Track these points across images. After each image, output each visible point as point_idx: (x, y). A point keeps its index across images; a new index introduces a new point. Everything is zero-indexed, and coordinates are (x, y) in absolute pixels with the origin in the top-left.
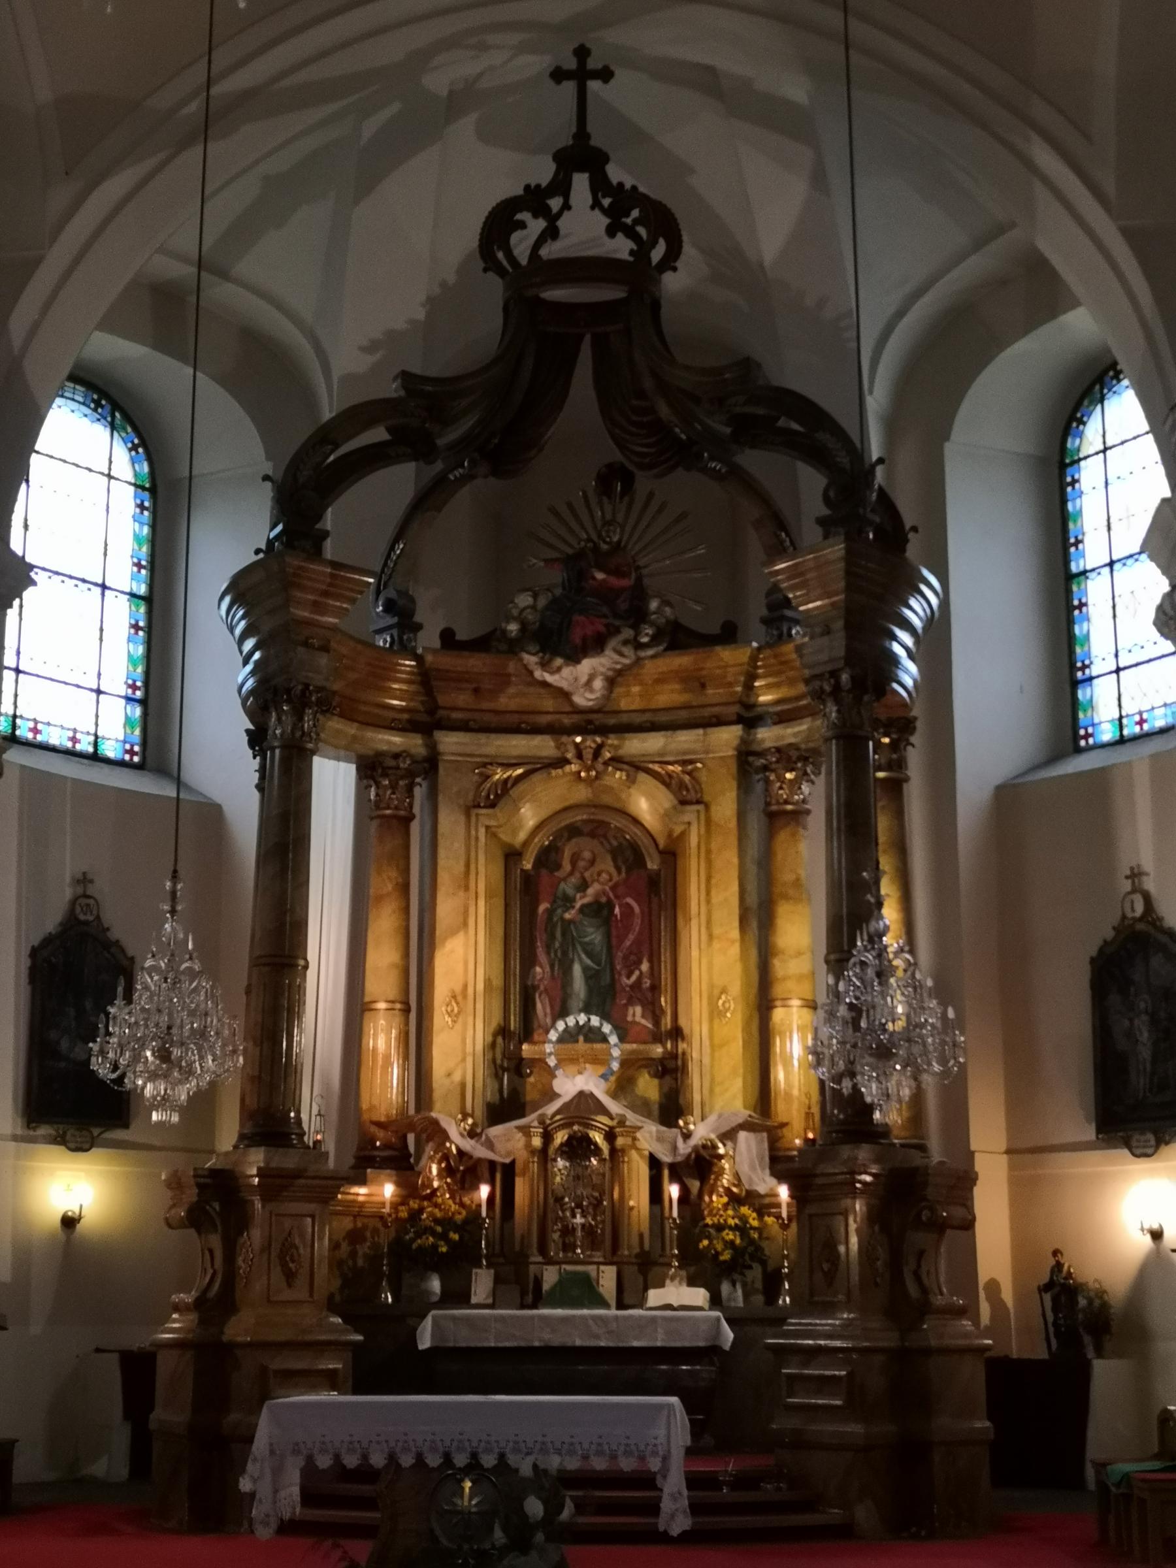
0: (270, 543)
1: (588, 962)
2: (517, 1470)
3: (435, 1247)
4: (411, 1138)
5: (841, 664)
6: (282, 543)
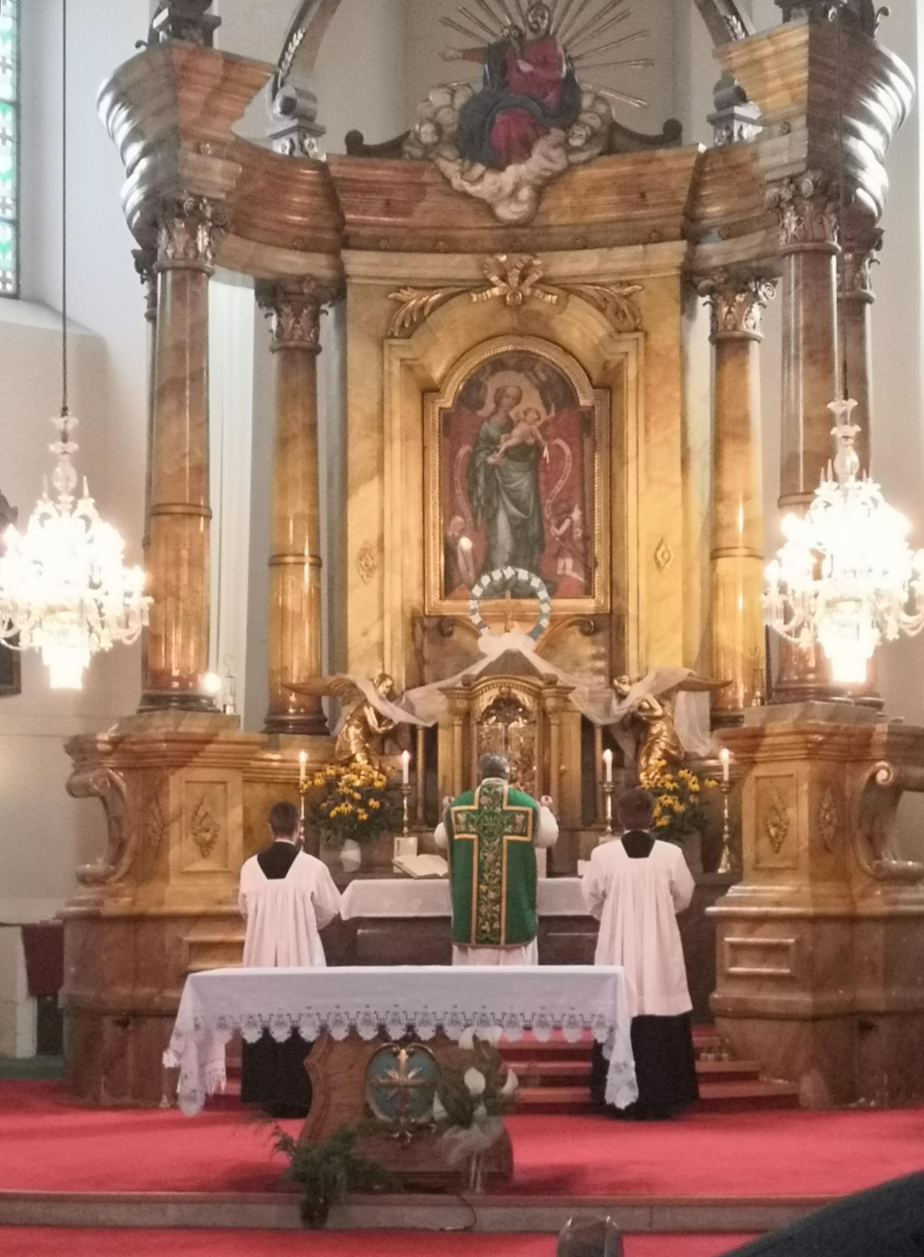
0: (153, 34)
1: (514, 510)
2: (456, 1043)
3: (354, 814)
4: (325, 701)
5: (801, 167)
6: (168, 32)
